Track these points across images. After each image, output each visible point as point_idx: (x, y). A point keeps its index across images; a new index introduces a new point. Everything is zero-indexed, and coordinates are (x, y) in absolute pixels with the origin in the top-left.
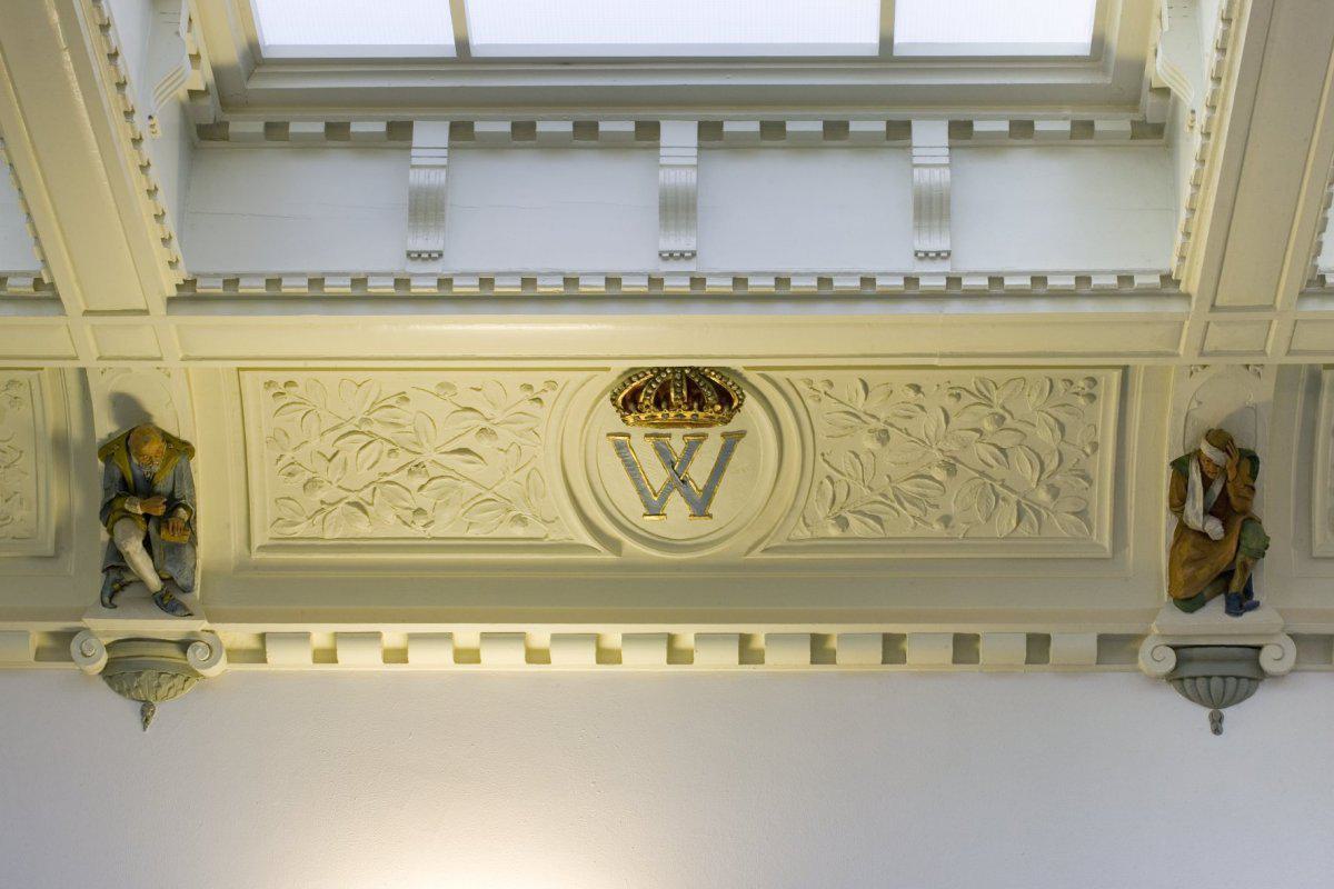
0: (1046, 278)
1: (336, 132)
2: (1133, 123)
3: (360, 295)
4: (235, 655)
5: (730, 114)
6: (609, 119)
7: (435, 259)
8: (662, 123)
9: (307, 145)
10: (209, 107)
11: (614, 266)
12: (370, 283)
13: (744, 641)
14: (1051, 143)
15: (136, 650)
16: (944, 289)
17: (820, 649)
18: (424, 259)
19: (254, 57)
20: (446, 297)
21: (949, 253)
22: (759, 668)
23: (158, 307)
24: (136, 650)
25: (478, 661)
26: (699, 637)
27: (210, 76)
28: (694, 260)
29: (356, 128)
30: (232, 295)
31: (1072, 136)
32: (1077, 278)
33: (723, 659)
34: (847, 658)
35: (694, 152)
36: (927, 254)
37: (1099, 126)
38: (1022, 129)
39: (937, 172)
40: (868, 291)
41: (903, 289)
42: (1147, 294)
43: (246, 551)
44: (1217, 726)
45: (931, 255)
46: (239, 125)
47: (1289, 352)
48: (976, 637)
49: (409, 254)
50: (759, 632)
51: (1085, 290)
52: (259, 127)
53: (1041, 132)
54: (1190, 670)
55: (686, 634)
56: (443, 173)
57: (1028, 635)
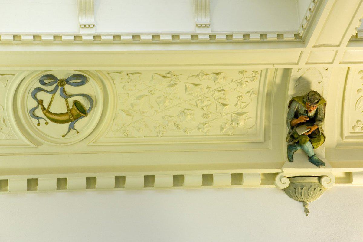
0: (140, 36)
4: (339, 180)
15: (301, 181)
24: (301, 181)
28: (94, 28)
41: (152, 40)
42: (126, 43)
43: (340, 138)
45: (86, 26)
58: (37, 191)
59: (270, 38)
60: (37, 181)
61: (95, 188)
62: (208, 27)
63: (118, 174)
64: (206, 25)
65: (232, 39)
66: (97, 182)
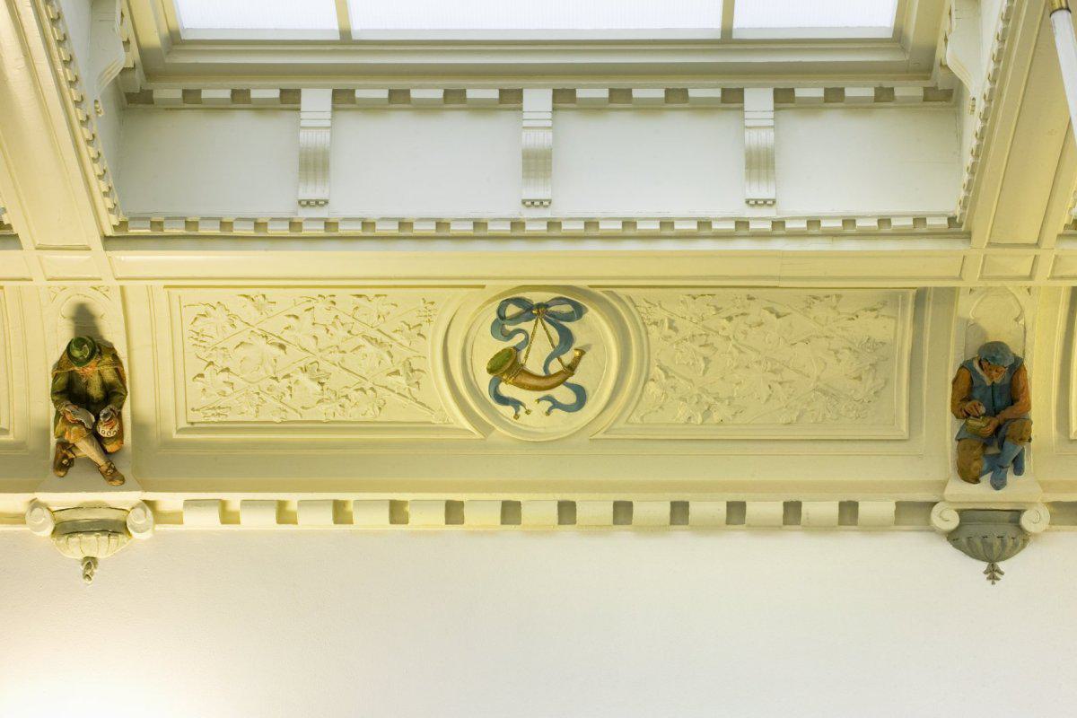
1: (834, 96)
2: (926, 90)
3: (260, 234)
5: (416, 83)
6: (420, 87)
7: (322, 205)
8: (303, 90)
9: (217, 108)
10: (138, 78)
11: (481, 212)
12: (304, 227)
13: (281, 505)
14: (858, 106)
16: (621, 231)
17: (340, 512)
18: (760, 205)
19: (174, 39)
20: (331, 233)
21: (774, 202)
22: (177, 528)
23: (97, 244)
25: (181, 522)
26: (245, 503)
27: (137, 56)
28: (774, 207)
29: (255, 94)
30: (158, 238)
31: (826, 99)
32: (808, 222)
33: (264, 521)
34: (417, 519)
35: (771, 115)
36: (308, 203)
37: (898, 92)
38: (239, 97)
39: (763, 133)
40: (480, 230)
44: (993, 574)
46: (168, 92)
47: (981, 278)
48: (462, 504)
49: (524, 202)
50: (293, 499)
51: (705, 232)
52: (178, 94)
53: (799, 98)
54: (971, 529)
55: (234, 499)
56: (549, 134)
57: (728, 503)
58: (800, 527)
59: (309, 230)
60: (858, 506)
61: (407, 523)
62: (546, 206)
63: (678, 497)
64: (533, 203)
65: (162, 230)
66: (634, 511)
